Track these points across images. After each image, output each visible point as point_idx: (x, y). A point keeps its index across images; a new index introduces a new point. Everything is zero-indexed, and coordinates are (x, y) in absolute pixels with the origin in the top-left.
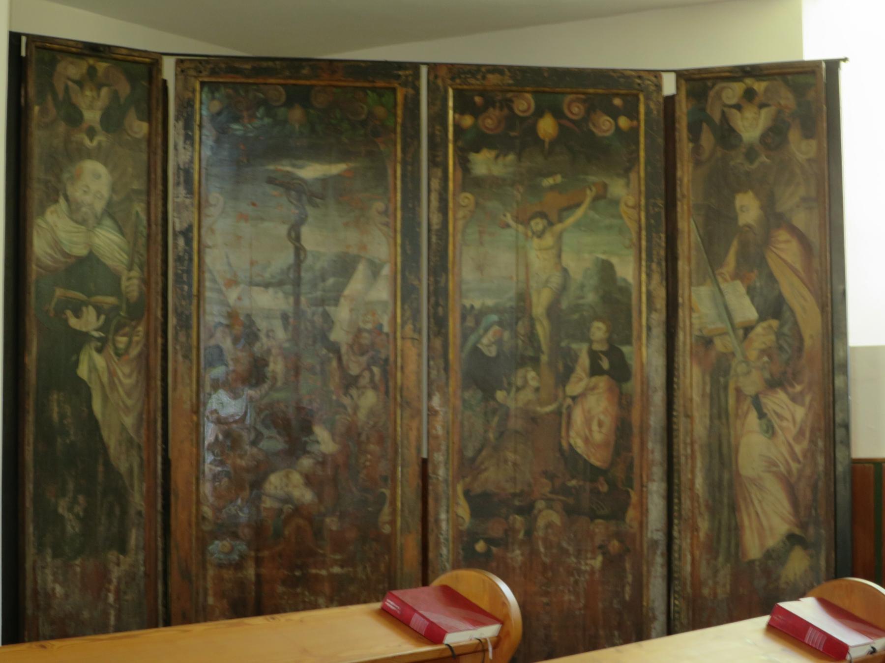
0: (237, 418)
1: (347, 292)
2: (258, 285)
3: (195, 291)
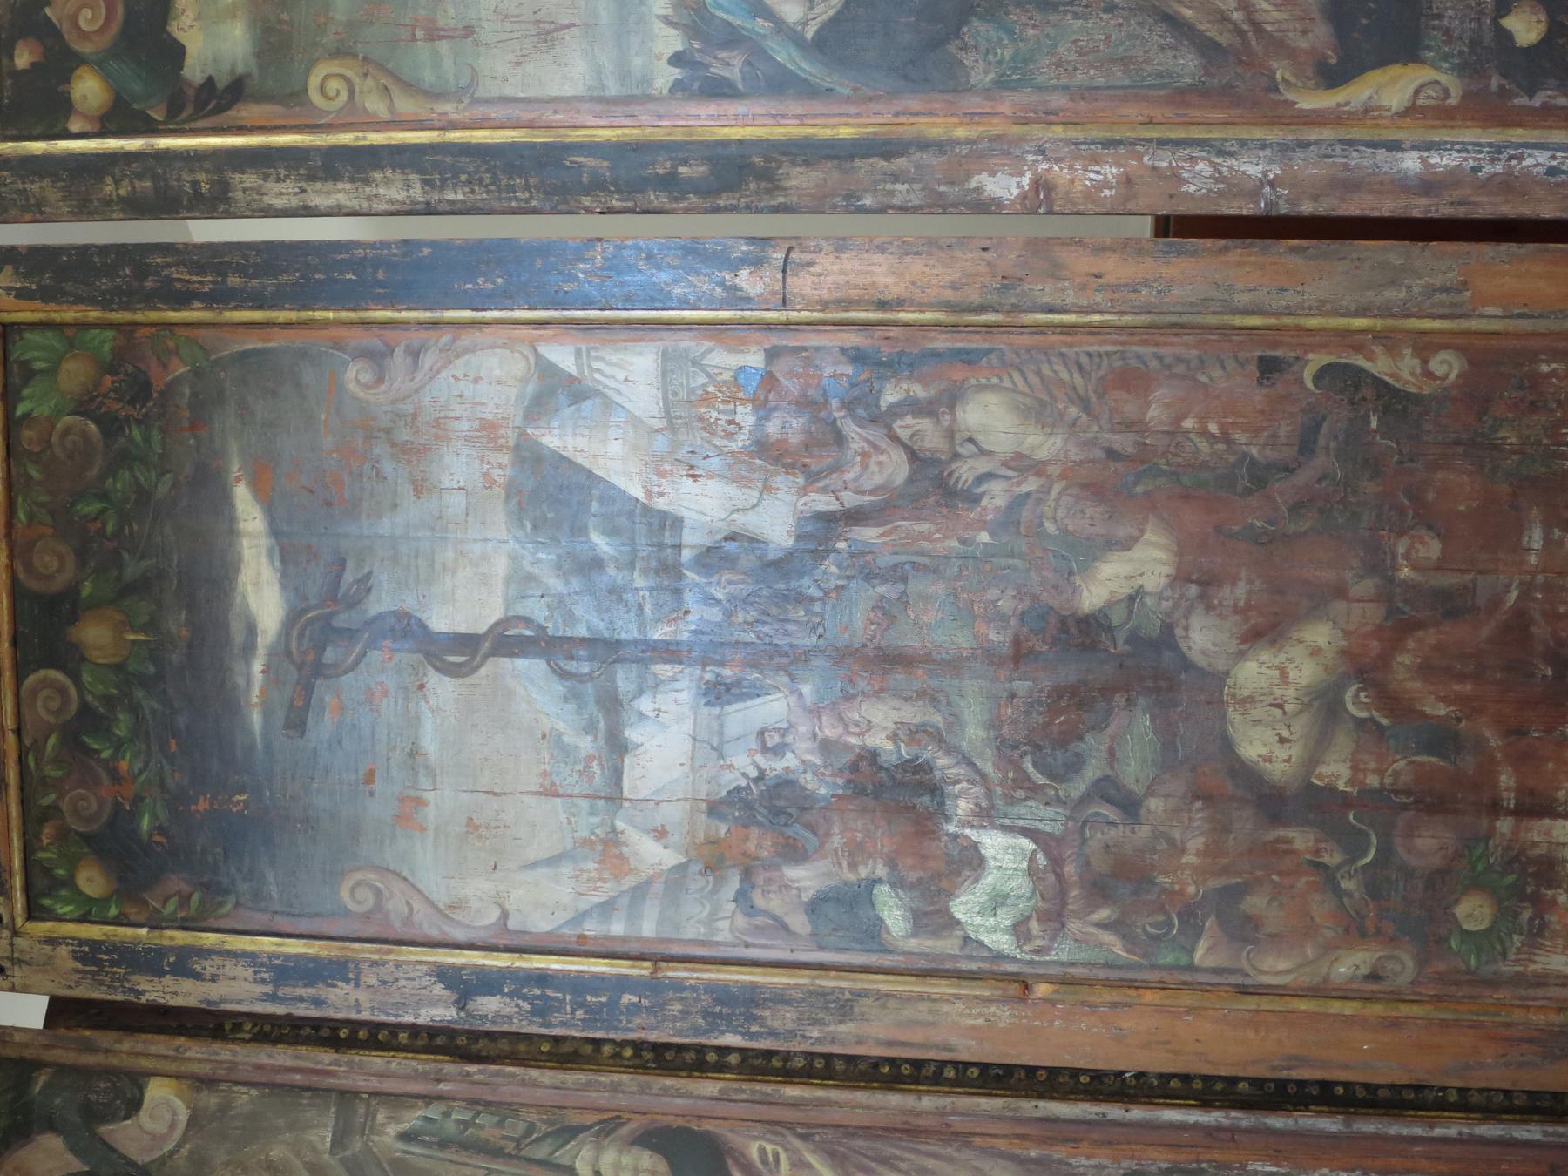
1: (637, 491)
2: (617, 774)
3: (642, 970)
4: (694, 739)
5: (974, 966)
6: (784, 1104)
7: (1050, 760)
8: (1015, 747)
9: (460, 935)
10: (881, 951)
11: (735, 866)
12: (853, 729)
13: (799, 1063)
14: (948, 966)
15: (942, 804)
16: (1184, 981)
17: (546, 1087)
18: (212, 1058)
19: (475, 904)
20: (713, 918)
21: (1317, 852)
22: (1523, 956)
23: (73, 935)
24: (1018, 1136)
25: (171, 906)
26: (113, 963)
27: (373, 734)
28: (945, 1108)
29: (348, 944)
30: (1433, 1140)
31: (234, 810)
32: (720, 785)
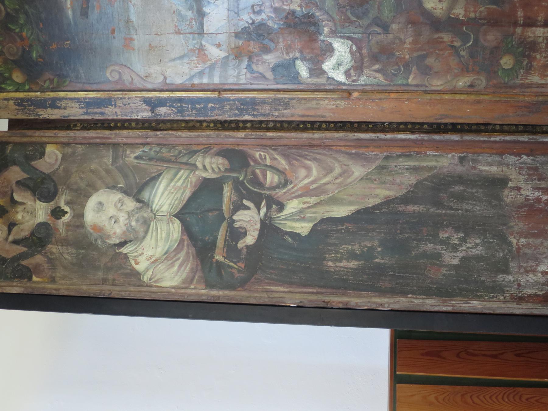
0: (354, 48)
2: (201, 25)
3: (215, 95)
4: (229, 10)
5: (331, 87)
6: (267, 139)
7: (357, 11)
8: (344, 7)
9: (150, 86)
10: (299, 84)
11: (245, 56)
12: (285, 3)
13: (271, 125)
14: (322, 88)
15: (318, 29)
16: (405, 90)
17: (184, 138)
18: (67, 136)
19: (154, 75)
20: (238, 76)
21: (452, 42)
22: (524, 77)
23: (14, 97)
24: (348, 146)
25: (47, 84)
26: (29, 106)
27: (113, 16)
28: (323, 137)
29: (111, 92)
30: (490, 141)
31: (66, 47)
32: (238, 27)
